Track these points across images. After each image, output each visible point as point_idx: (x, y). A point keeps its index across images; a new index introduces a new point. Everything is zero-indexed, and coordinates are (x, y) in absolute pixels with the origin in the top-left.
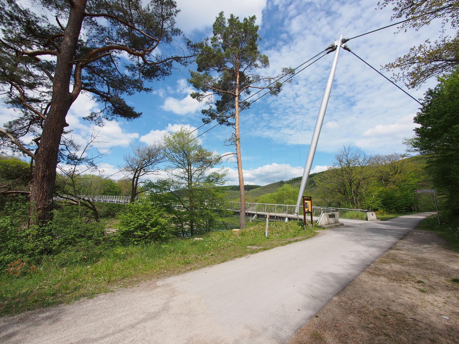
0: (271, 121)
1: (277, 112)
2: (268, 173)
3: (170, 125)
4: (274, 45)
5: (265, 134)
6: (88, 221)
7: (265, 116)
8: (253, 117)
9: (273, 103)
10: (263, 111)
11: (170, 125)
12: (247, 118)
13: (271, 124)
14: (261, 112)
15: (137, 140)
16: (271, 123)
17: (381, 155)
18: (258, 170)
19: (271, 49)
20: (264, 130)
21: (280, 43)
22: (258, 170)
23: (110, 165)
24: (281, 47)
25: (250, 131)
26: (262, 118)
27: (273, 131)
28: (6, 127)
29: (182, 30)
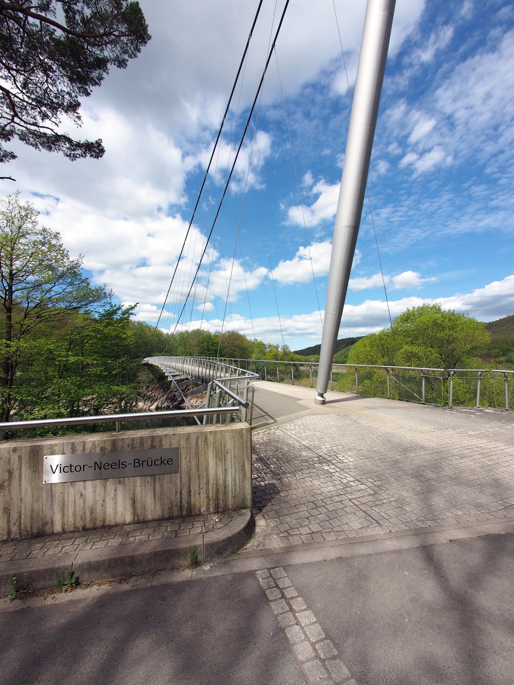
0: (494, 196)
1: (505, 176)
2: (498, 298)
3: (301, 248)
4: (482, 43)
5: (481, 224)
6: (186, 388)
7: (479, 190)
8: (450, 200)
9: (493, 160)
10: (469, 183)
11: (301, 248)
12: (436, 204)
13: (494, 203)
14: (465, 185)
15: (266, 278)
16: (492, 200)
17: (404, 312)
18: (477, 294)
19: (473, 56)
20: (478, 217)
21: (495, 32)
22: (477, 294)
23: (241, 316)
24: (499, 40)
25: (447, 226)
26: (470, 198)
27: (501, 215)
28: (31, 530)
29: (2, 506)
